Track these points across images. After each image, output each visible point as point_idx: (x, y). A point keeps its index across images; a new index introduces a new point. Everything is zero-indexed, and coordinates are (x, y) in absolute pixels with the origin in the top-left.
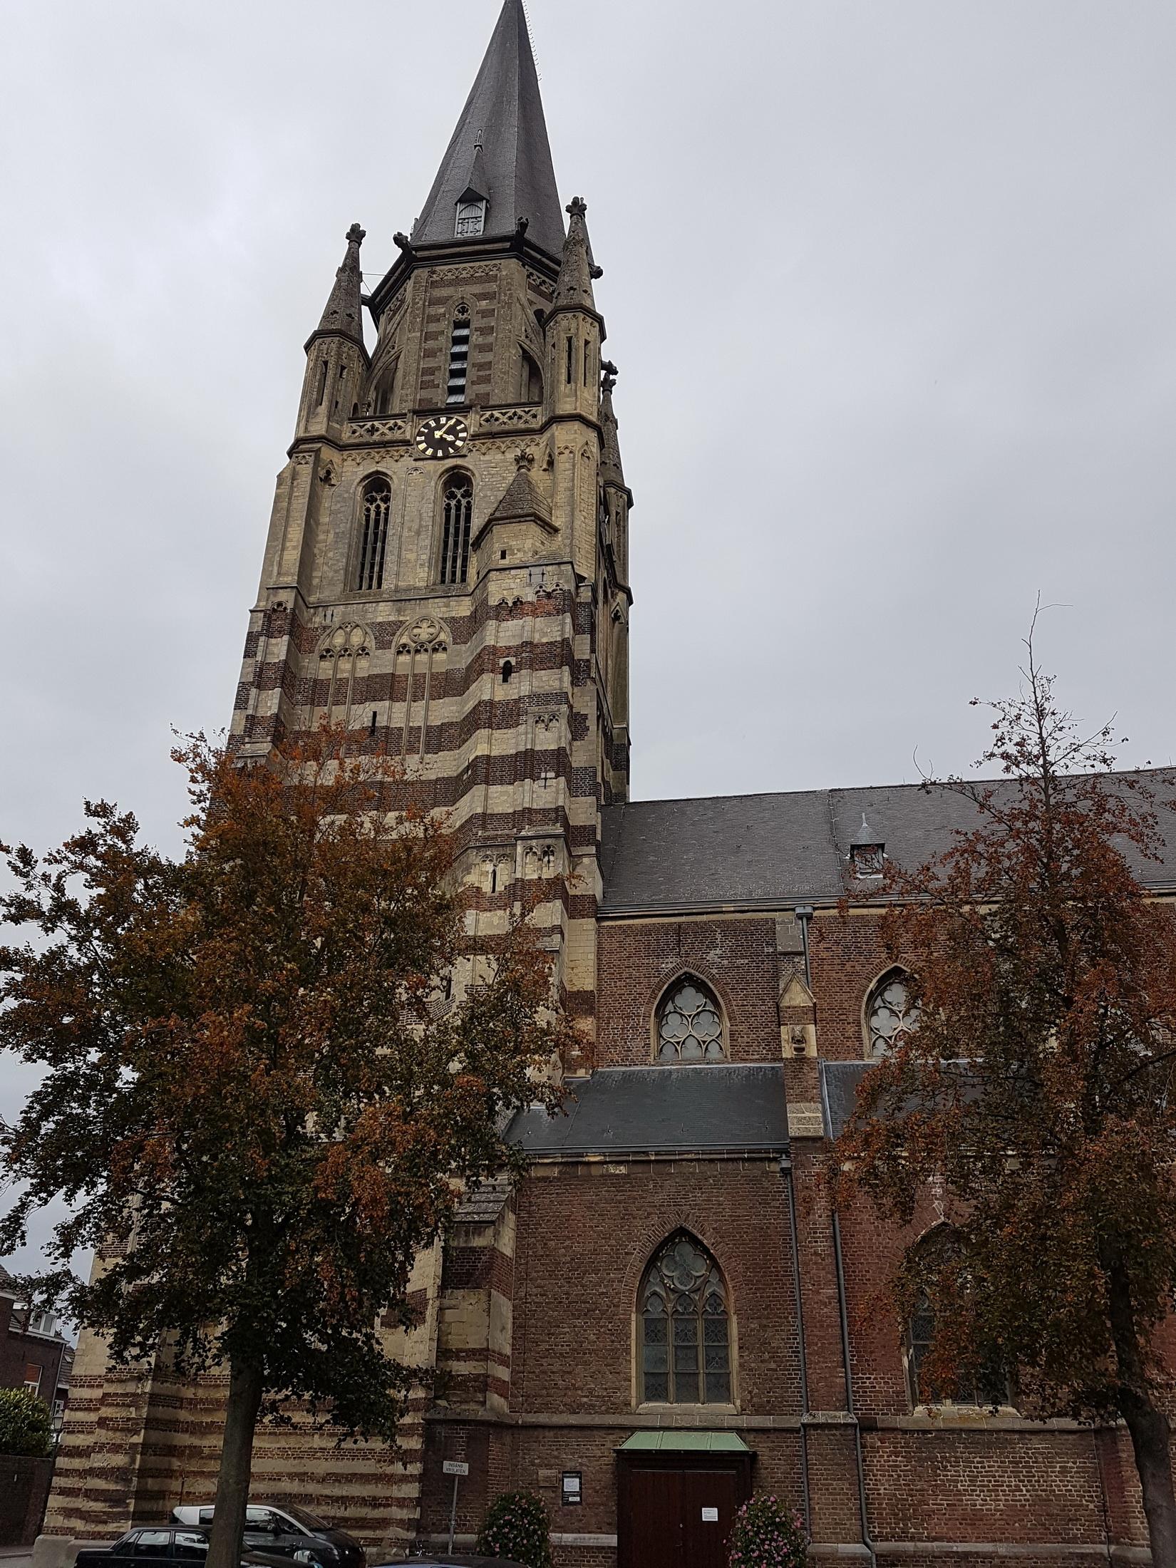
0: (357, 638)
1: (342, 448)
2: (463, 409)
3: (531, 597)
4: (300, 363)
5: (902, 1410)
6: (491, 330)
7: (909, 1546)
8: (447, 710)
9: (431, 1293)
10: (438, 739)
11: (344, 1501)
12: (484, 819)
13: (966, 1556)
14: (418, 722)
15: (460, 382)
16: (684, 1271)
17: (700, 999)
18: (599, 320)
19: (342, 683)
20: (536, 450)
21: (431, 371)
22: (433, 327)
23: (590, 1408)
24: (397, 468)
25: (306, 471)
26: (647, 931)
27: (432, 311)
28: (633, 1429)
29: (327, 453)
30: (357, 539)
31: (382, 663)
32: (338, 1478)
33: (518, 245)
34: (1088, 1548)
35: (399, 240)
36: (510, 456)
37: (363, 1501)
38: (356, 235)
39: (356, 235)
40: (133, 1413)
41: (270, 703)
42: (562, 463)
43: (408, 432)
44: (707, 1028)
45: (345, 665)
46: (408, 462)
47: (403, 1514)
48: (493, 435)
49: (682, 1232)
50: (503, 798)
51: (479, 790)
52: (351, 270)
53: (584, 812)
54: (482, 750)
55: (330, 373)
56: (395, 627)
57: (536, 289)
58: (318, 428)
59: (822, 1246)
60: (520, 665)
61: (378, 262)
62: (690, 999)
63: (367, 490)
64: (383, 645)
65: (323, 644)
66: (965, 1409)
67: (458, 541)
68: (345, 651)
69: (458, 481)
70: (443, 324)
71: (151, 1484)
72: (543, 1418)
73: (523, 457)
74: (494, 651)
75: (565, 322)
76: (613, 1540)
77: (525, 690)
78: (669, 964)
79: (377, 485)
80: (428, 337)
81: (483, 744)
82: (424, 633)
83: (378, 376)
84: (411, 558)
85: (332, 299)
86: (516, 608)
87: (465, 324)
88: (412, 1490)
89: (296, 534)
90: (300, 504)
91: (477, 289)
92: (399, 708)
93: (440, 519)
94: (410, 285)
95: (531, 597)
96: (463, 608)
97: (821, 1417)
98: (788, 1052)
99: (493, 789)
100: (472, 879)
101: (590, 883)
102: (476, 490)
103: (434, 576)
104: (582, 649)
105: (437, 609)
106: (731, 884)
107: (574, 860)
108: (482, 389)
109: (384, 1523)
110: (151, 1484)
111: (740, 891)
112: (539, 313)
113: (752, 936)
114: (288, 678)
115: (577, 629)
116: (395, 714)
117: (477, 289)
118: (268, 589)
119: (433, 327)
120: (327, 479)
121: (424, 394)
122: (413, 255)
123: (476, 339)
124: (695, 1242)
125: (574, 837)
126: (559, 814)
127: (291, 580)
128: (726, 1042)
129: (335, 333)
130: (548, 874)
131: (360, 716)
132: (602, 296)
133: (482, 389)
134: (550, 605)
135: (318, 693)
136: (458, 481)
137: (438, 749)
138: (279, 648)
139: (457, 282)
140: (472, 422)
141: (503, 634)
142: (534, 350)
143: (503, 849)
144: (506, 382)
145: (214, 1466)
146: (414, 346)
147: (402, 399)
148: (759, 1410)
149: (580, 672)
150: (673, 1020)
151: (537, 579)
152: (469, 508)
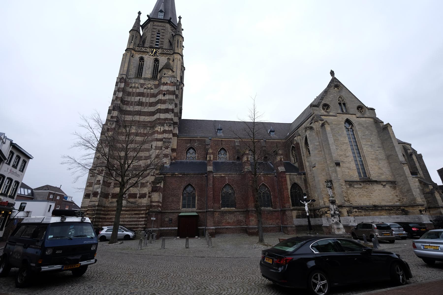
0: (137, 85)
1: (136, 51)
2: (159, 48)
3: (169, 82)
4: (128, 35)
5: (220, 209)
6: (164, 36)
7: (219, 227)
8: (153, 100)
9: (147, 193)
10: (151, 104)
11: (131, 225)
12: (159, 119)
13: (227, 228)
14: (147, 101)
15: (158, 44)
16: (189, 189)
17: (193, 151)
18: (183, 38)
19: (134, 93)
20: (171, 58)
21: (153, 41)
22: (153, 33)
23: (174, 210)
24: (146, 57)
25: (129, 55)
26: (185, 140)
27: (153, 30)
28: (180, 212)
29: (133, 52)
30: (138, 67)
31: (141, 90)
32: (130, 221)
33: (169, 22)
34: (243, 226)
35: (148, 16)
36: (166, 58)
37: (134, 225)
38: (140, 13)
39: (140, 13)
40: (93, 212)
41: (120, 95)
42: (175, 61)
43: (148, 50)
44: (194, 155)
45: (134, 90)
46: (148, 56)
47: (141, 226)
48: (163, 54)
49: (189, 185)
50: (163, 116)
51: (158, 114)
52: (138, 19)
53: (176, 120)
54: (159, 107)
55: (134, 38)
56: (144, 84)
57: (172, 30)
58: (131, 47)
59: (211, 186)
60: (167, 94)
61: (144, 19)
62: (191, 151)
63: (140, 59)
64: (142, 87)
65: (130, 86)
66: (228, 208)
67: (156, 70)
68: (134, 87)
69: (156, 61)
70: (155, 33)
71: (96, 223)
72: (166, 211)
73: (169, 58)
74: (162, 91)
75: (177, 37)
76: (177, 228)
77: (167, 98)
78: (189, 145)
79: (142, 59)
80: (152, 34)
81: (159, 106)
82: (149, 86)
83: (143, 40)
84: (147, 72)
85: (135, 24)
86: (166, 84)
87: (159, 34)
88: (143, 223)
89: (126, 65)
90: (127, 60)
91: (162, 28)
92: (144, 99)
93: (153, 67)
94: (149, 25)
95: (169, 82)
96: (157, 82)
97: (209, 210)
98: (208, 159)
99: (161, 114)
100: (156, 129)
101: (176, 131)
102: (160, 63)
103: (151, 76)
104: (177, 92)
105: (152, 82)
106: (199, 134)
107: (174, 128)
108: (162, 45)
109: (138, 228)
110: (96, 223)
111: (200, 135)
112: (172, 35)
113: (202, 142)
114: (124, 90)
115: (177, 89)
116: (144, 99)
117: (162, 28)
118: (120, 74)
119: (153, 33)
120: (132, 56)
121: (151, 44)
122: (150, 19)
123: (161, 36)
124: (191, 186)
125: (175, 123)
126: (172, 119)
127: (125, 73)
128: (197, 157)
129: (134, 31)
130: (170, 129)
131: (137, 99)
132: (184, 34)
133: (162, 45)
134: (172, 84)
135: (129, 94)
136: (156, 61)
137: (151, 106)
138: (122, 85)
139: (158, 26)
140: (160, 51)
141: (164, 88)
142: (171, 40)
143: (163, 125)
144: (166, 45)
145: (121, 223)
146: (150, 36)
147: (147, 44)
148: (199, 209)
149: (177, 96)
150: (189, 154)
151: (170, 79)
152: (158, 65)
